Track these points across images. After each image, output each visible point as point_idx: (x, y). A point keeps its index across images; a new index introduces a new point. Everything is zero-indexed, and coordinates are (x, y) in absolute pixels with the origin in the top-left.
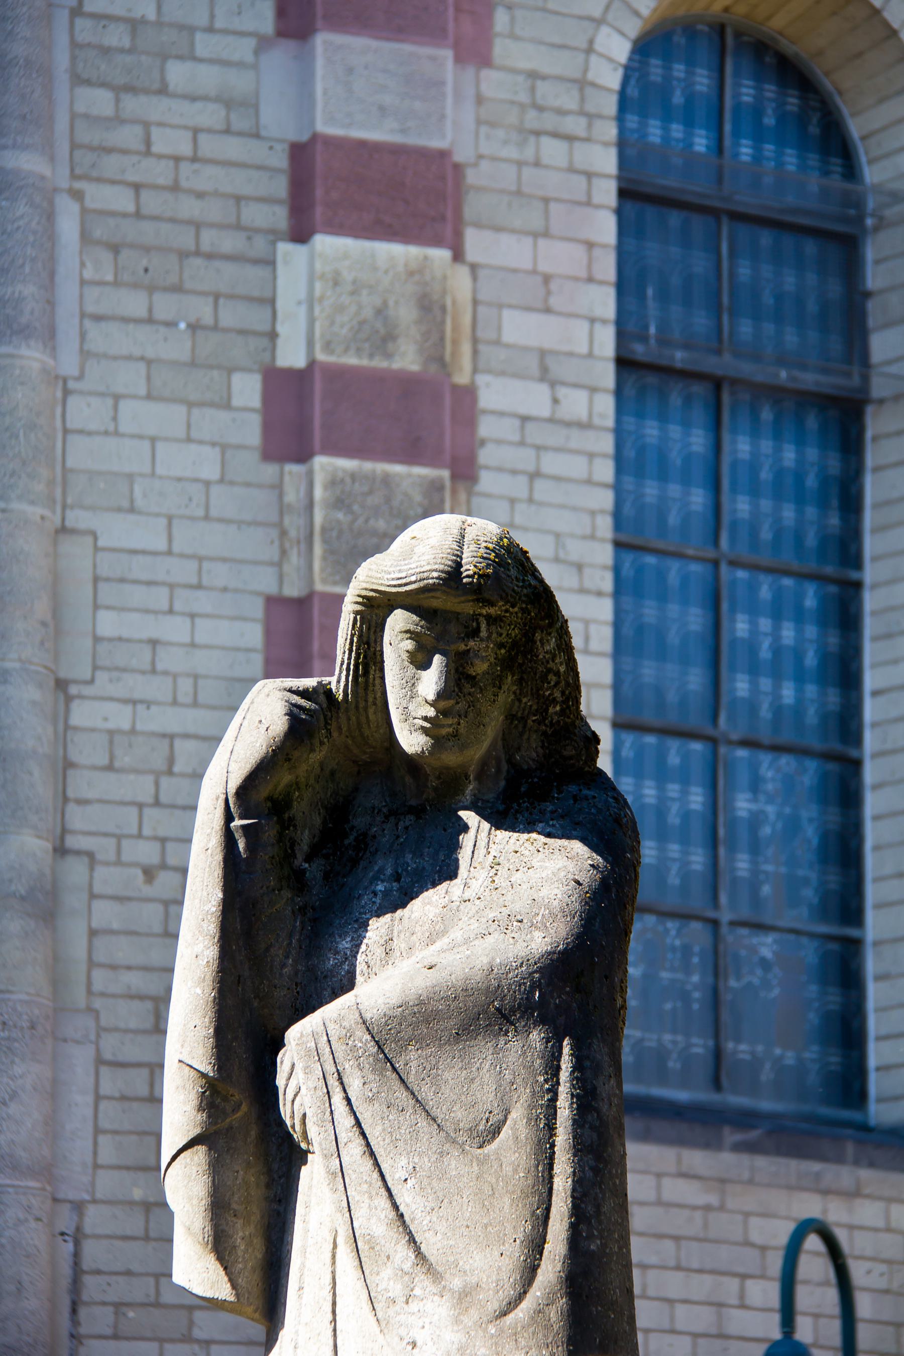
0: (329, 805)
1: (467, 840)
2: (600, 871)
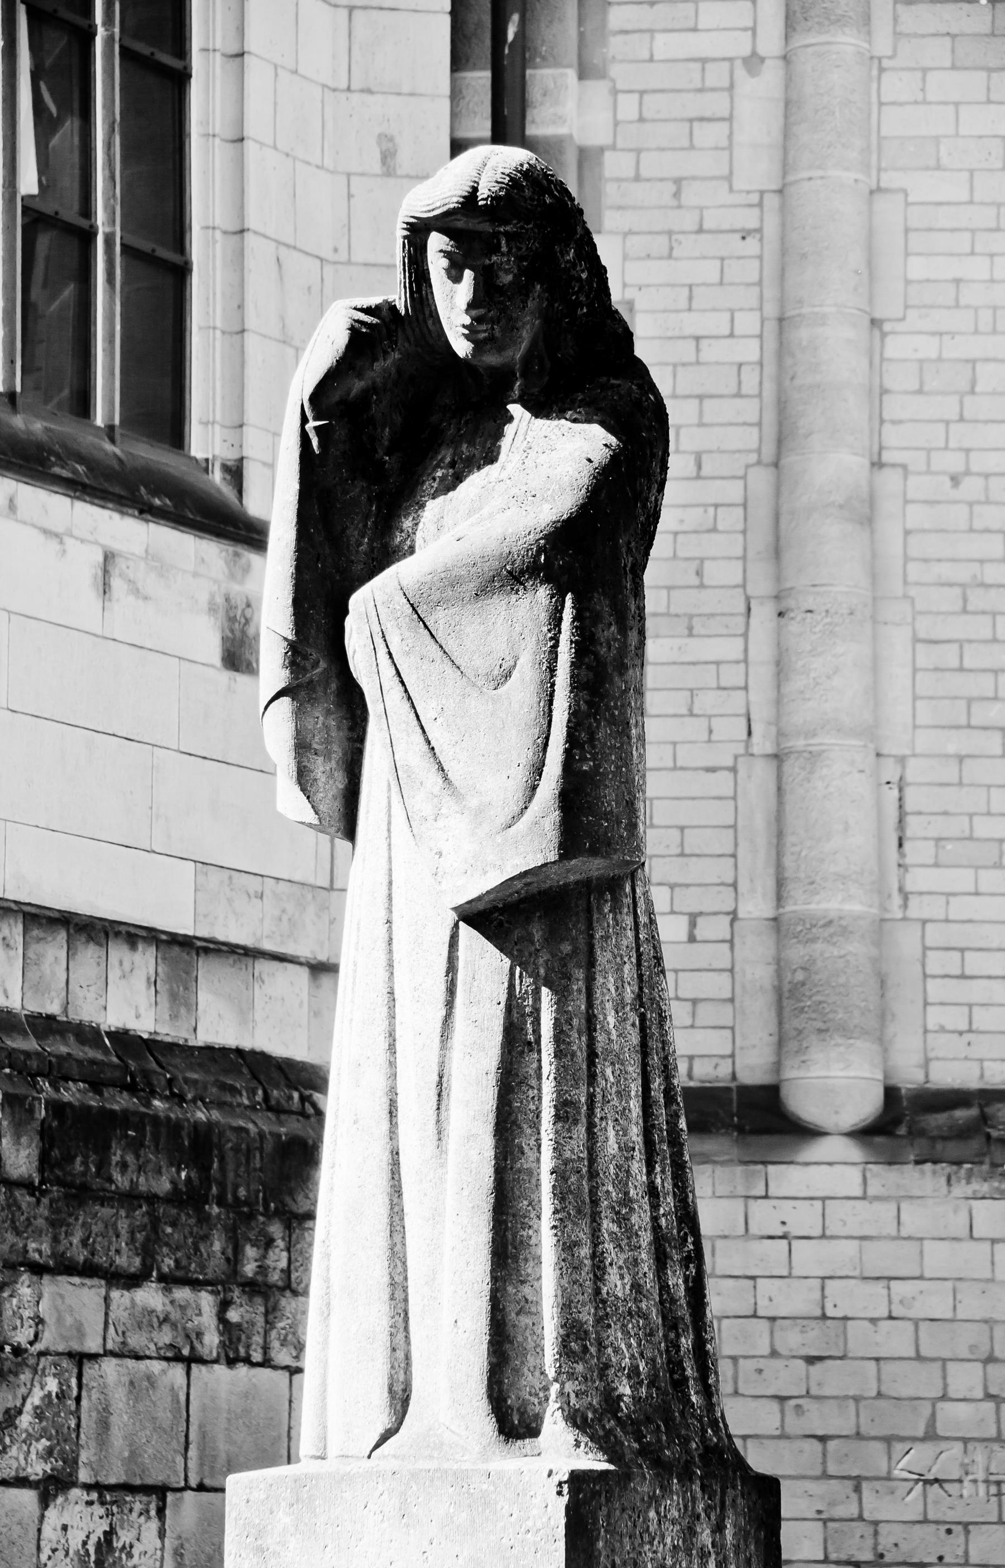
1: (509, 429)
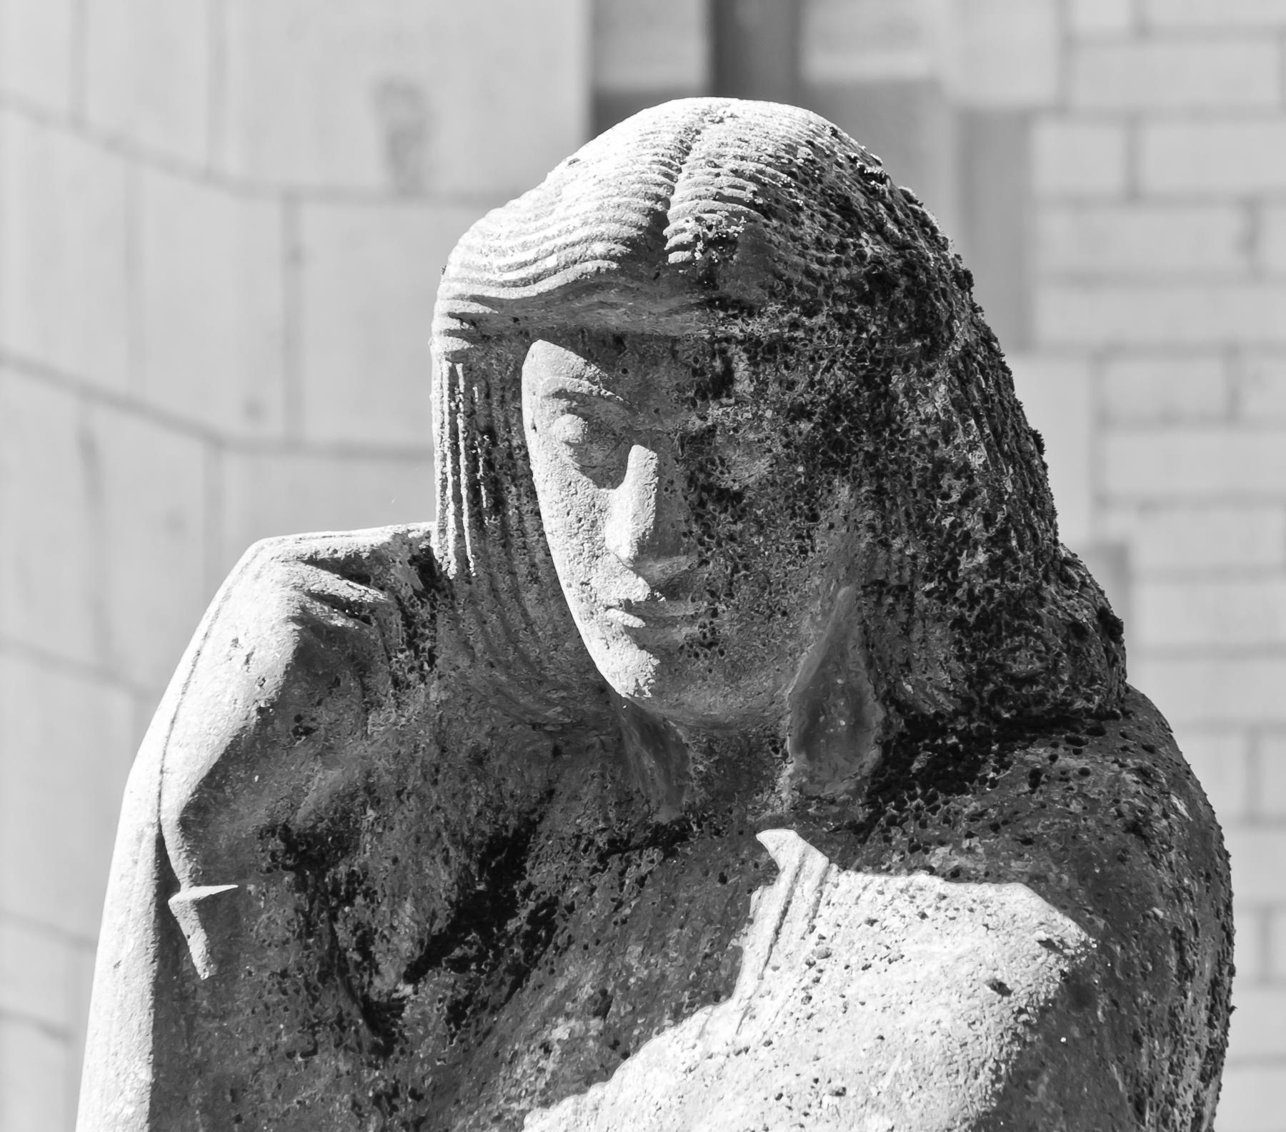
0: (477, 838)
1: (766, 903)
2: (1066, 957)
